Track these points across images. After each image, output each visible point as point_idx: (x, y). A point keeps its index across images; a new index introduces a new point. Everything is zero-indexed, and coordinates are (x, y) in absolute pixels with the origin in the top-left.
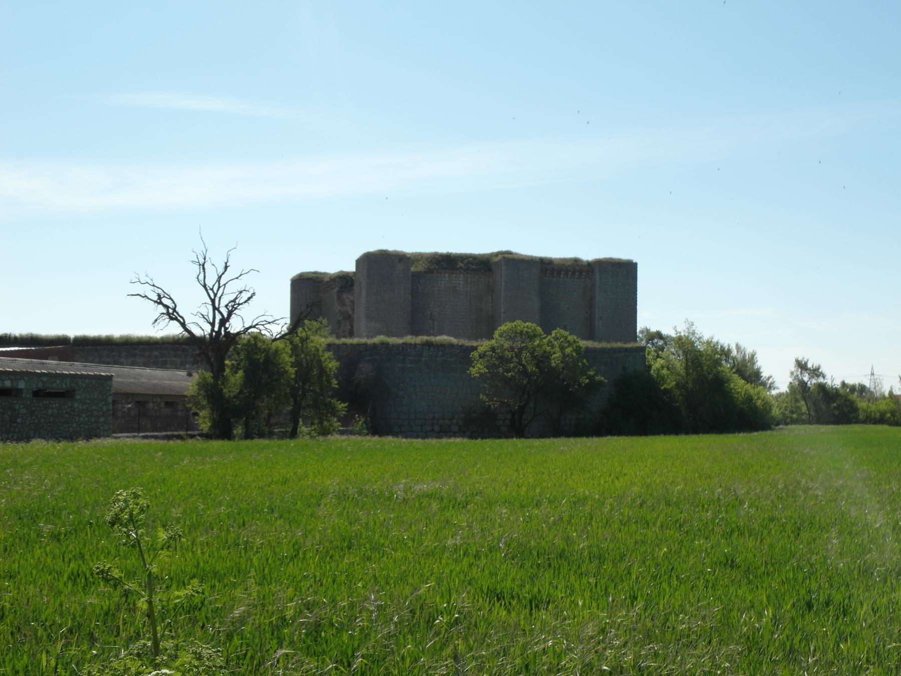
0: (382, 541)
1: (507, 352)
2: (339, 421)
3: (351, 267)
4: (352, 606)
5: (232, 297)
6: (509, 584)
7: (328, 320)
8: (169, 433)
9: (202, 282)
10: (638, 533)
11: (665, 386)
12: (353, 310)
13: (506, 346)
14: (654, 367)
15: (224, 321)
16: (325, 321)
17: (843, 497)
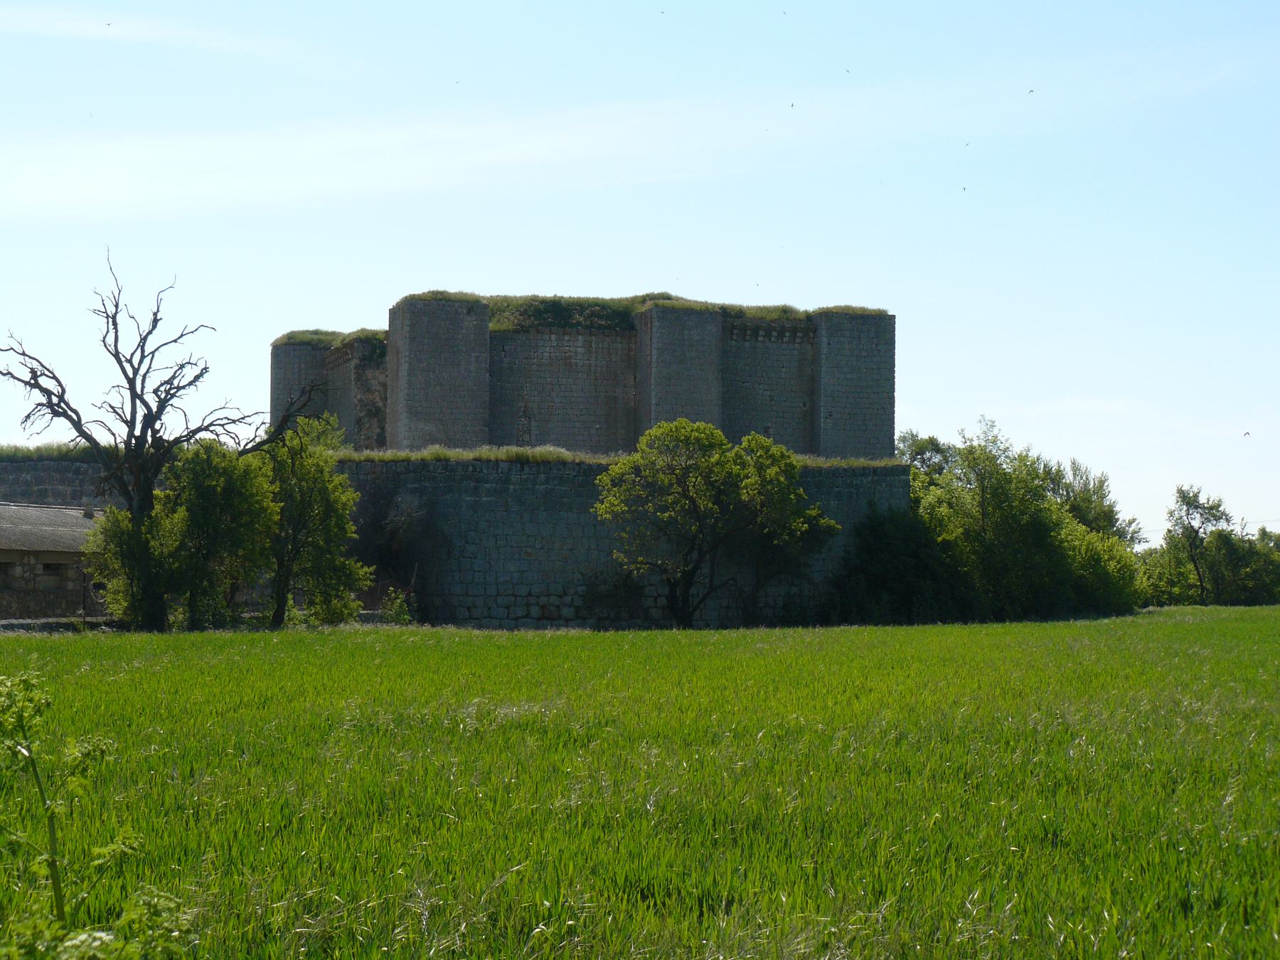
0: (439, 801)
1: (661, 475)
4: (386, 907)
5: (167, 375)
9: (112, 348)
10: (892, 788)
12: (385, 399)
13: (660, 464)
15: (151, 419)
16: (334, 420)
17: (1255, 726)
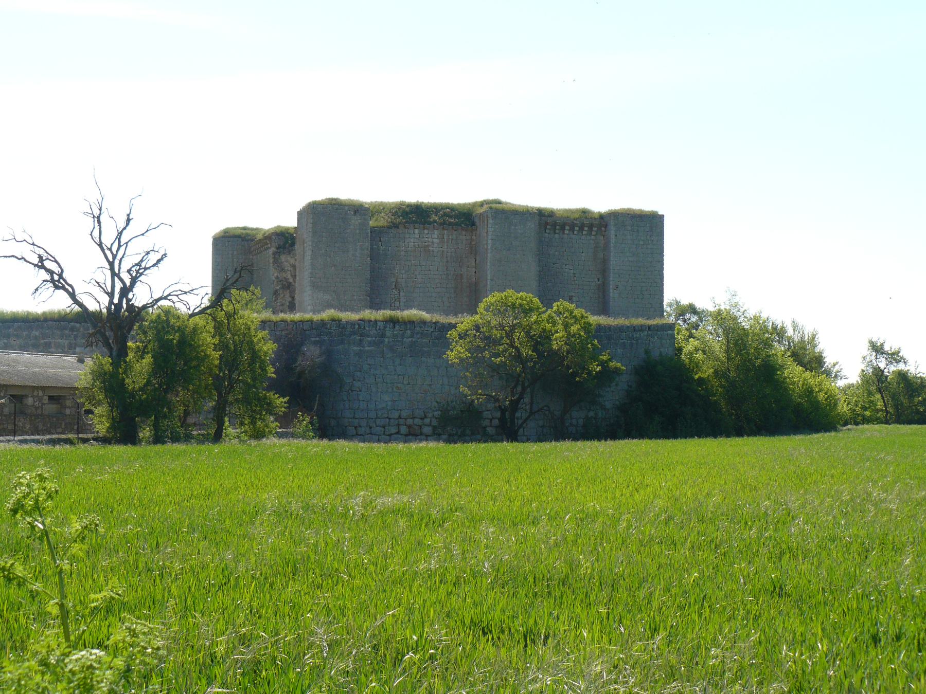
0: (336, 565)
1: (494, 331)
2: (276, 420)
3: (291, 222)
4: (299, 640)
6: (497, 614)
7: (262, 290)
8: (54, 436)
9: (97, 240)
10: (663, 555)
11: (700, 374)
12: (294, 277)
14: (685, 351)
15: (125, 291)
16: (258, 292)
